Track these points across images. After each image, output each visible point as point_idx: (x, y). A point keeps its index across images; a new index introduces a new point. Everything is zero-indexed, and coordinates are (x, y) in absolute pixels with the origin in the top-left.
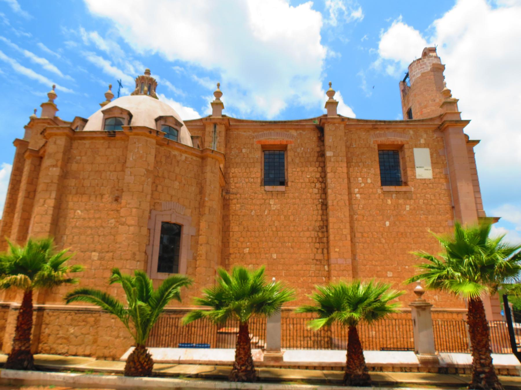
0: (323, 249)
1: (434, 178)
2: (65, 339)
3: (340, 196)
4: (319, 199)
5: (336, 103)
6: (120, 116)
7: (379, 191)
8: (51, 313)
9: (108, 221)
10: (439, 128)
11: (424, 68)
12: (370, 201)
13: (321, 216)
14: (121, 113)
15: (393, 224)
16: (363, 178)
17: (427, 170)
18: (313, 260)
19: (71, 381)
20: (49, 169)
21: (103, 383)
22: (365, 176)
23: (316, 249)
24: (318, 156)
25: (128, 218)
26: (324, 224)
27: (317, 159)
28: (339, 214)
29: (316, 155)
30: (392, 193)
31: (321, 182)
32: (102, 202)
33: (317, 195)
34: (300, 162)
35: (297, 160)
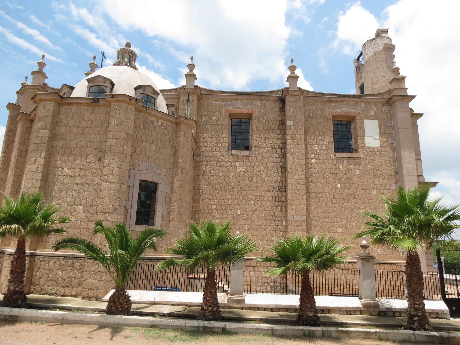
0: (281, 207)
2: (54, 281)
4: (279, 163)
7: (333, 157)
8: (41, 259)
9: (92, 178)
10: (387, 102)
13: (281, 178)
16: (318, 145)
19: (60, 318)
21: (87, 320)
24: (279, 125)
25: (110, 176)
29: (278, 123)
31: (281, 148)
32: (87, 162)
33: (278, 159)
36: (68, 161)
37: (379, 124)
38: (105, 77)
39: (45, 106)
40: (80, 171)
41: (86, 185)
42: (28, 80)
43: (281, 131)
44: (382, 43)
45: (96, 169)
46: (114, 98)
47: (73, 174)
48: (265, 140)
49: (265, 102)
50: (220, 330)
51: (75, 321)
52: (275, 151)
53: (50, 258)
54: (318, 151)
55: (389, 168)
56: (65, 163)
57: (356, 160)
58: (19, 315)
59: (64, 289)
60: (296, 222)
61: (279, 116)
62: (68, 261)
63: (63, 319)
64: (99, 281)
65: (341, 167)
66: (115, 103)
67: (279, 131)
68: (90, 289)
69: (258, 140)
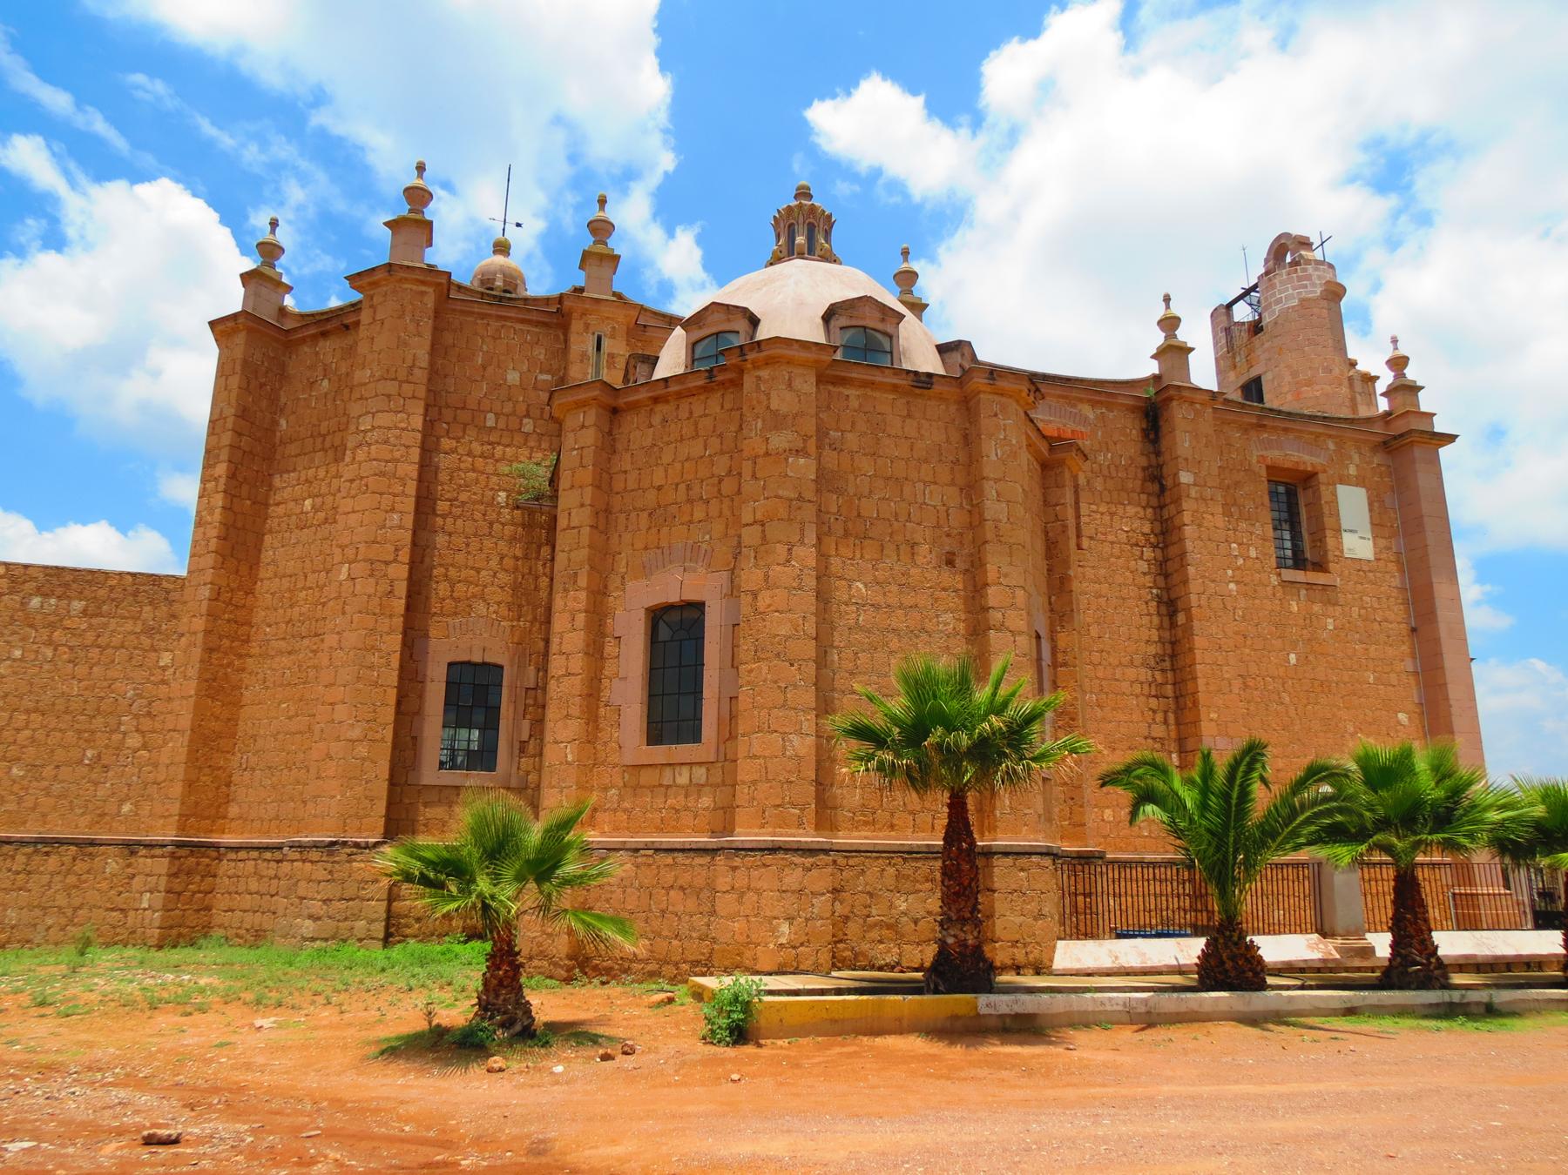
0: (1166, 712)
1: (1378, 559)
2: (889, 927)
3: (1213, 585)
4: (1151, 588)
5: (1185, 350)
6: (880, 326)
7: (1274, 580)
8: (841, 861)
9: (937, 616)
10: (1385, 443)
11: (1306, 287)
12: (1257, 601)
13: (1158, 630)
14: (883, 320)
15: (1304, 660)
16: (1239, 544)
17: (1364, 538)
18: (1146, 738)
19: (1142, 1009)
20: (786, 460)
21: (1207, 1008)
22: (1245, 540)
23: (1150, 713)
24: (1144, 481)
25: (1009, 612)
26: (1164, 650)
27: (1143, 485)
28: (1214, 630)
29: (1140, 475)
30: (1298, 585)
31: (1155, 547)
32: (915, 565)
33: (1147, 577)
34: (1105, 489)
35: (1098, 484)
36: (861, 558)
37: (1369, 498)
38: (884, 305)
39: (789, 379)
40: (901, 592)
41: (924, 636)
42: (278, 230)
43: (1151, 498)
44: (1319, 277)
45: (944, 589)
46: (747, 357)
47: (880, 599)
48: (1112, 520)
49: (1104, 410)
50: (1482, 1010)
51: (1178, 1014)
52: (1138, 553)
53: (867, 857)
54: (1240, 561)
55: (1395, 616)
56: (852, 565)
57: (1326, 590)
58: (1036, 1012)
59: (920, 948)
60: (1221, 754)
61: (1142, 454)
62: (919, 865)
63: (1149, 1013)
64: (1035, 919)
65: (1295, 608)
66: (990, 397)
67: (1144, 497)
68: (1017, 942)
69: (1096, 519)
